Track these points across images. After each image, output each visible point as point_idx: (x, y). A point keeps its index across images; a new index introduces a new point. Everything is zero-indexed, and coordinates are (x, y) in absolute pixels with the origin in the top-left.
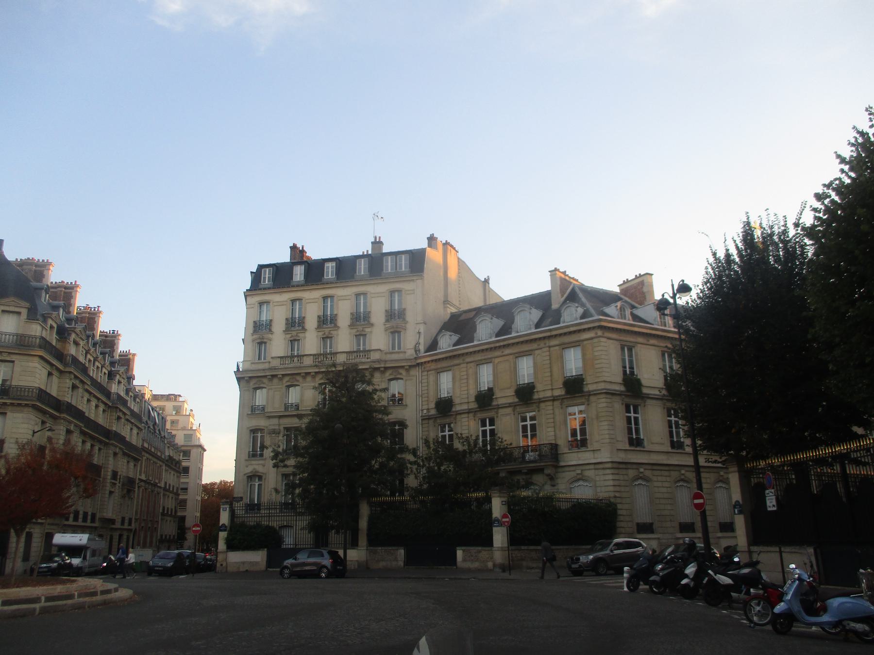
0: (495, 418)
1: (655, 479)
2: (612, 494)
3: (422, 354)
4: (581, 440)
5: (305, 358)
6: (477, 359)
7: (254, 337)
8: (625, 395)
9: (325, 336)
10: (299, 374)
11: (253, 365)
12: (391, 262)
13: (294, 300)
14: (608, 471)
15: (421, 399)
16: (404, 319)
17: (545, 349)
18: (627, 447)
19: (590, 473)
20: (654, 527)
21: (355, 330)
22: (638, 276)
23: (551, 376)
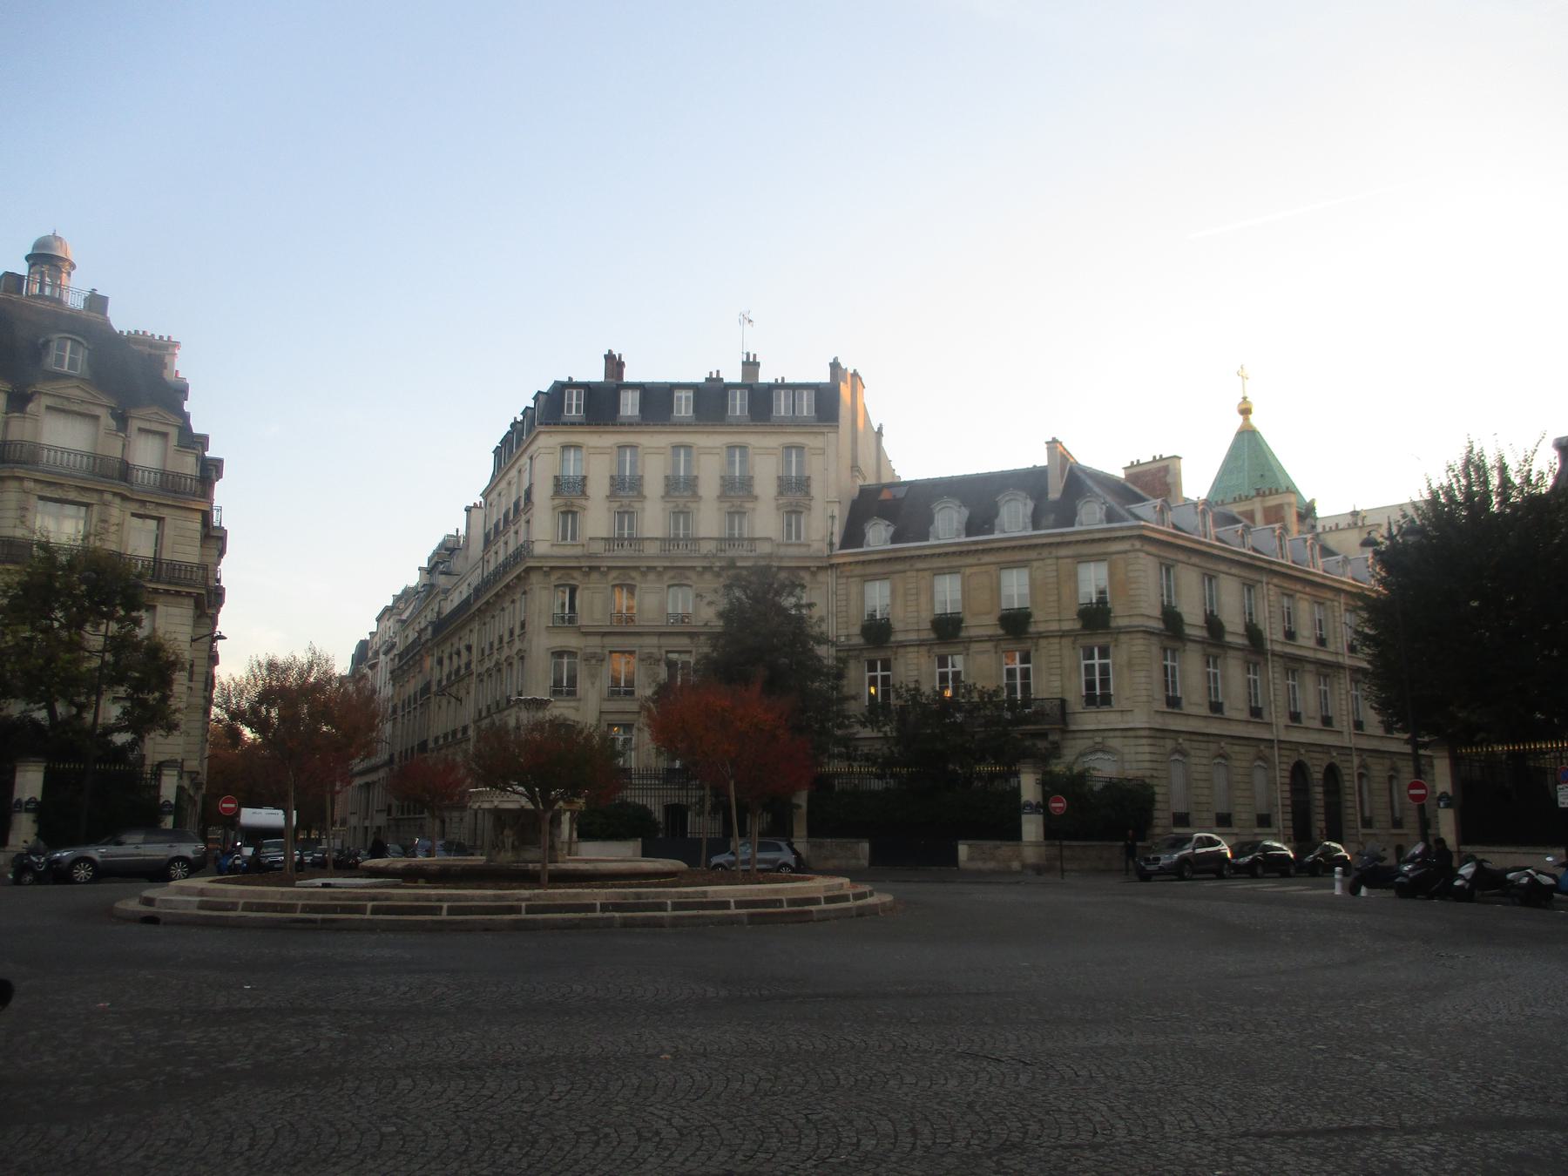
0: (892, 660)
1: (1193, 752)
2: (1148, 773)
4: (1102, 695)
5: (647, 543)
6: (935, 565)
7: (557, 502)
8: (1165, 635)
9: (676, 510)
10: (636, 568)
11: (555, 548)
12: (802, 405)
13: (731, 447)
14: (1144, 741)
15: (835, 620)
16: (807, 494)
17: (1049, 561)
19: (1115, 743)
20: (1191, 818)
21: (618, 504)
22: (1135, 463)
23: (1059, 600)
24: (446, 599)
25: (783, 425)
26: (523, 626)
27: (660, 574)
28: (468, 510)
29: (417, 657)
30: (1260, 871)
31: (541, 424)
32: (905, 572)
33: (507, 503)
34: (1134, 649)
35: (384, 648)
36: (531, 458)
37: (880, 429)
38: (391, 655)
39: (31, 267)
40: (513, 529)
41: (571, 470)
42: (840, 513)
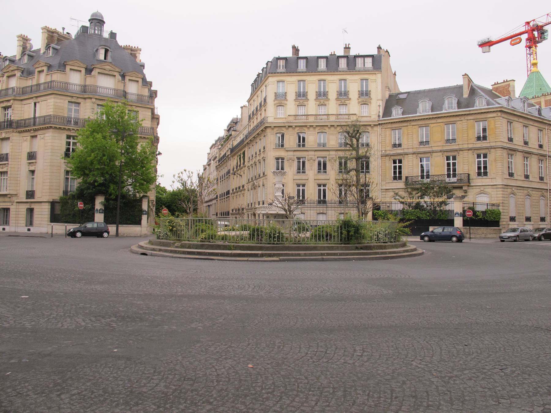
1: (518, 194)
3: (381, 119)
7: (276, 102)
18: (508, 177)
21: (299, 102)
24: (235, 140)
25: (360, 72)
26: (264, 148)
27: (315, 128)
28: (242, 108)
29: (225, 161)
30: (543, 238)
31: (269, 73)
32: (407, 126)
33: (256, 104)
34: (497, 154)
35: (213, 158)
36: (266, 86)
37: (395, 73)
38: (215, 161)
39: (91, 23)
40: (259, 113)
41: (281, 90)
42: (382, 104)
